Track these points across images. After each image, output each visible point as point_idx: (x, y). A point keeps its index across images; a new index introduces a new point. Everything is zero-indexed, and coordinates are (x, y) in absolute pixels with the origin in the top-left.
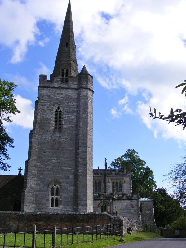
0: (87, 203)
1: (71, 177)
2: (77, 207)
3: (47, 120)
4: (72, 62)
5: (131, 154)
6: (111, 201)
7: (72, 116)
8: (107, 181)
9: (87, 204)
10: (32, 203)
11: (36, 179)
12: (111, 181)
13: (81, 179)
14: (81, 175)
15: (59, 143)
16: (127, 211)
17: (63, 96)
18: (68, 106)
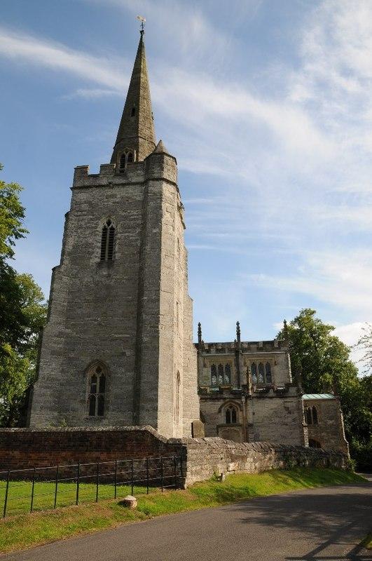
0: (159, 405)
1: (128, 353)
2: (138, 414)
3: (85, 247)
4: (142, 140)
5: (305, 319)
6: (243, 400)
7: (133, 235)
8: (241, 362)
9: (157, 408)
10: (51, 409)
11: (61, 359)
12: (248, 363)
13: (146, 356)
14: (148, 348)
15: (108, 287)
16: (277, 420)
17: (117, 201)
18: (126, 218)
